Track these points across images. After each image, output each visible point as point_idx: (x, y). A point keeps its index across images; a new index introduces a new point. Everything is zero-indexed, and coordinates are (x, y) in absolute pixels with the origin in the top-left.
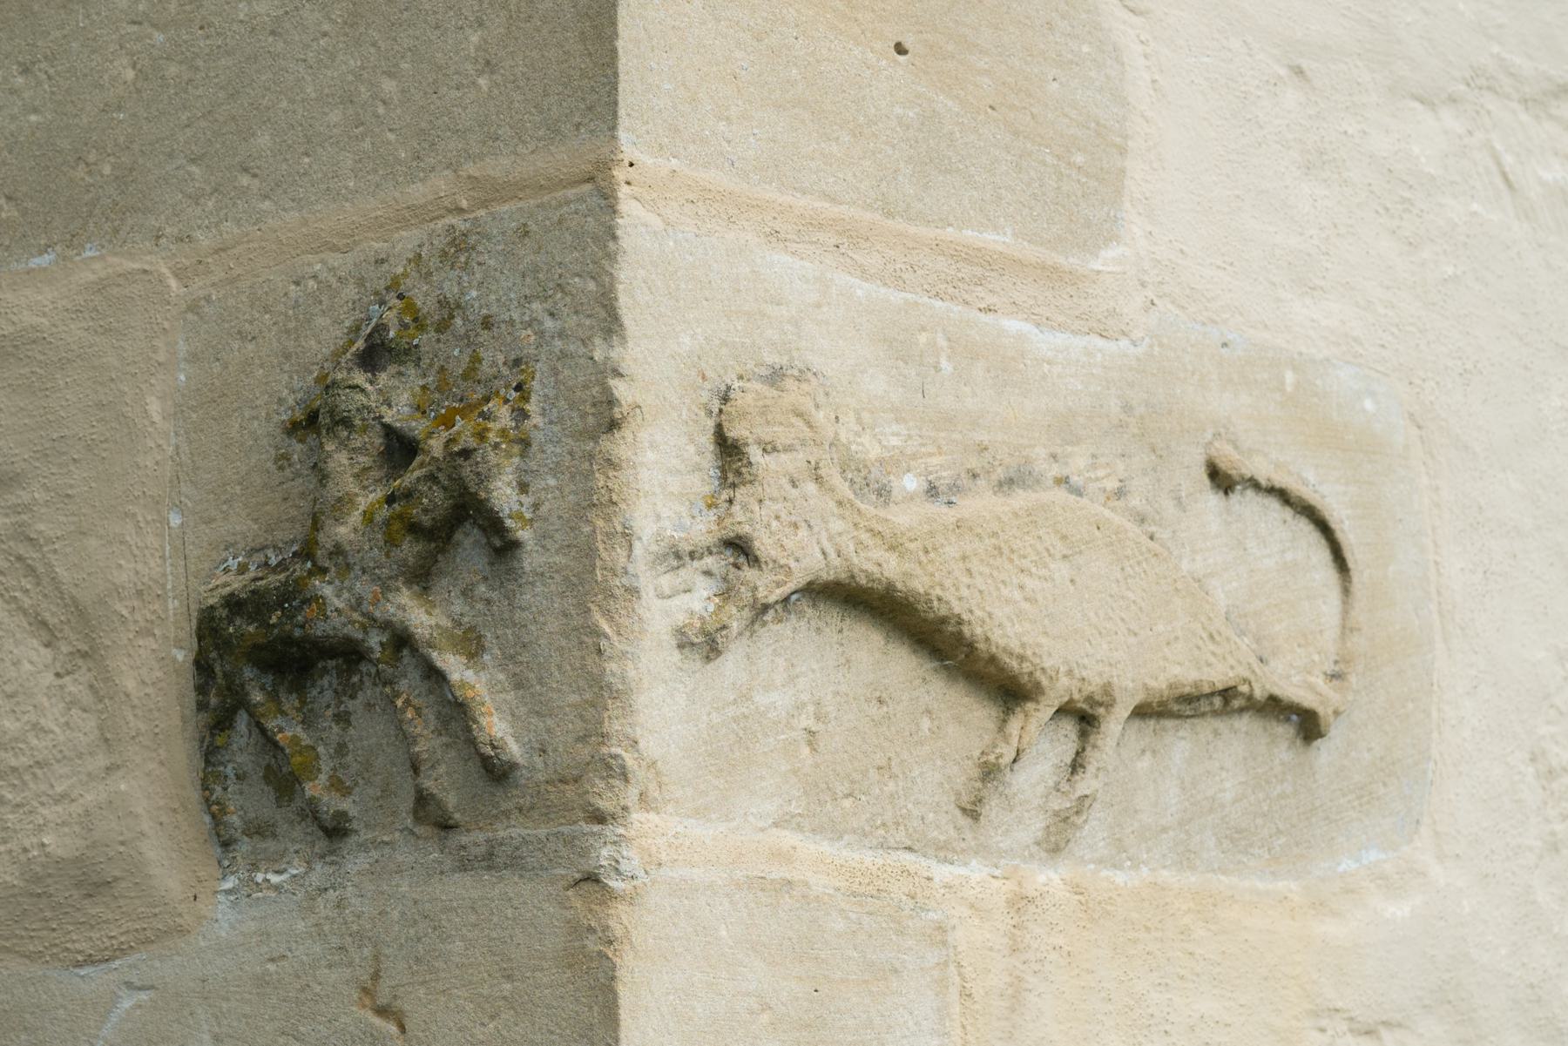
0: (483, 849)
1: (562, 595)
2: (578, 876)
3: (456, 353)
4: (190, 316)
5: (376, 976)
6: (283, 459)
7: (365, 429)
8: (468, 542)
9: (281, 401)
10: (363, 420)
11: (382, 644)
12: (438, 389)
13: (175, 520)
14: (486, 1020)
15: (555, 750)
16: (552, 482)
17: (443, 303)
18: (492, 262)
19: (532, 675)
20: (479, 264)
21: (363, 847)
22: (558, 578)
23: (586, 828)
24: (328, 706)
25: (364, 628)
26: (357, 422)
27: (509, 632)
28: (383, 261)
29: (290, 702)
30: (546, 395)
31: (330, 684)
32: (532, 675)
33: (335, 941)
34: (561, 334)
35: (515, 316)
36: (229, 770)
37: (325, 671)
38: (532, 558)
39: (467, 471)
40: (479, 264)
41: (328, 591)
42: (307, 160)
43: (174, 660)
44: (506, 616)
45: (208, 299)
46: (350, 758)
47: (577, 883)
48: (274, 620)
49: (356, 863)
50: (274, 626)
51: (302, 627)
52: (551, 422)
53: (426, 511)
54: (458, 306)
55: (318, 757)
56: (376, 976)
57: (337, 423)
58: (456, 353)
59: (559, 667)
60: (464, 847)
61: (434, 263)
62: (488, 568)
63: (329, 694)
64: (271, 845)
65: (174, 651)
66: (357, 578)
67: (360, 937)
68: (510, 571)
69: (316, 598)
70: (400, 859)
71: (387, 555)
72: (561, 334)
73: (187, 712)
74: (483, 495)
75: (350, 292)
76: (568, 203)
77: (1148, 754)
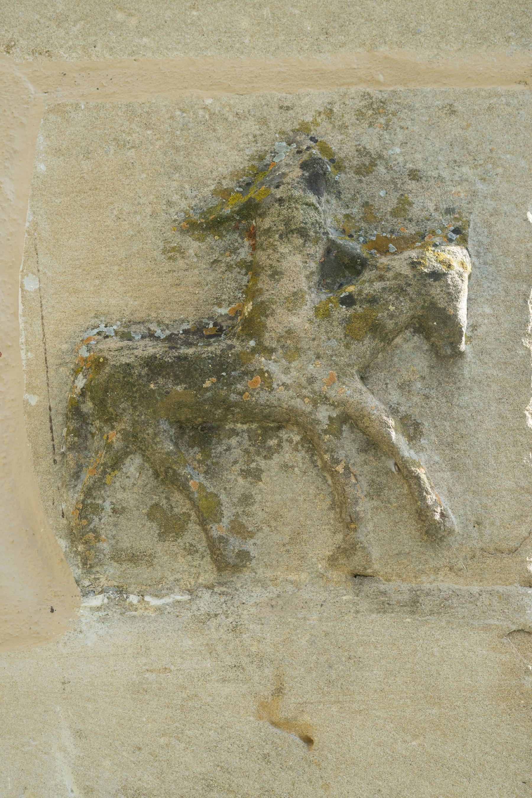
0: (407, 596)
1: (499, 401)
2: (514, 628)
3: (382, 193)
4: (52, 117)
5: (279, 691)
6: (173, 252)
7: (317, 241)
8: (407, 347)
9: (169, 203)
10: (316, 232)
11: (330, 418)
12: (364, 219)
13: (31, 284)
14: (408, 738)
15: (493, 524)
16: (488, 310)
17: (362, 152)
18: (416, 128)
19: (468, 461)
20: (402, 128)
21: (263, 583)
22: (494, 387)
23: (522, 590)
24: (235, 462)
25: (315, 404)
26: (312, 233)
27: (447, 424)
28: (288, 108)
29: (196, 453)
30: (479, 241)
31: (240, 443)
32: (468, 461)
33: (229, 660)
34: (494, 196)
35: (445, 174)
36: (107, 506)
37: (234, 432)
38: (471, 367)
39: (435, 290)
40: (402, 128)
41: (274, 368)
42: (195, 13)
43: (26, 403)
44: (444, 410)
45: (77, 107)
46: (255, 508)
47: (511, 634)
48: (207, 384)
49: (251, 595)
50: (207, 389)
51: (241, 394)
52: (485, 263)
53: (391, 316)
54: (380, 157)
55: (219, 504)
56: (279, 691)
57: (292, 231)
58: (382, 193)
59: (496, 458)
60: (384, 593)
61: (350, 118)
62: (427, 370)
63: (237, 452)
64: (144, 572)
65: (27, 396)
66: (310, 361)
67: (260, 660)
68: (449, 375)
69: (262, 372)
70: (306, 596)
71: (347, 346)
72: (494, 196)
73: (42, 449)
74: (451, 312)
75: (251, 126)
76: (498, 95)
77: (158, 612)
